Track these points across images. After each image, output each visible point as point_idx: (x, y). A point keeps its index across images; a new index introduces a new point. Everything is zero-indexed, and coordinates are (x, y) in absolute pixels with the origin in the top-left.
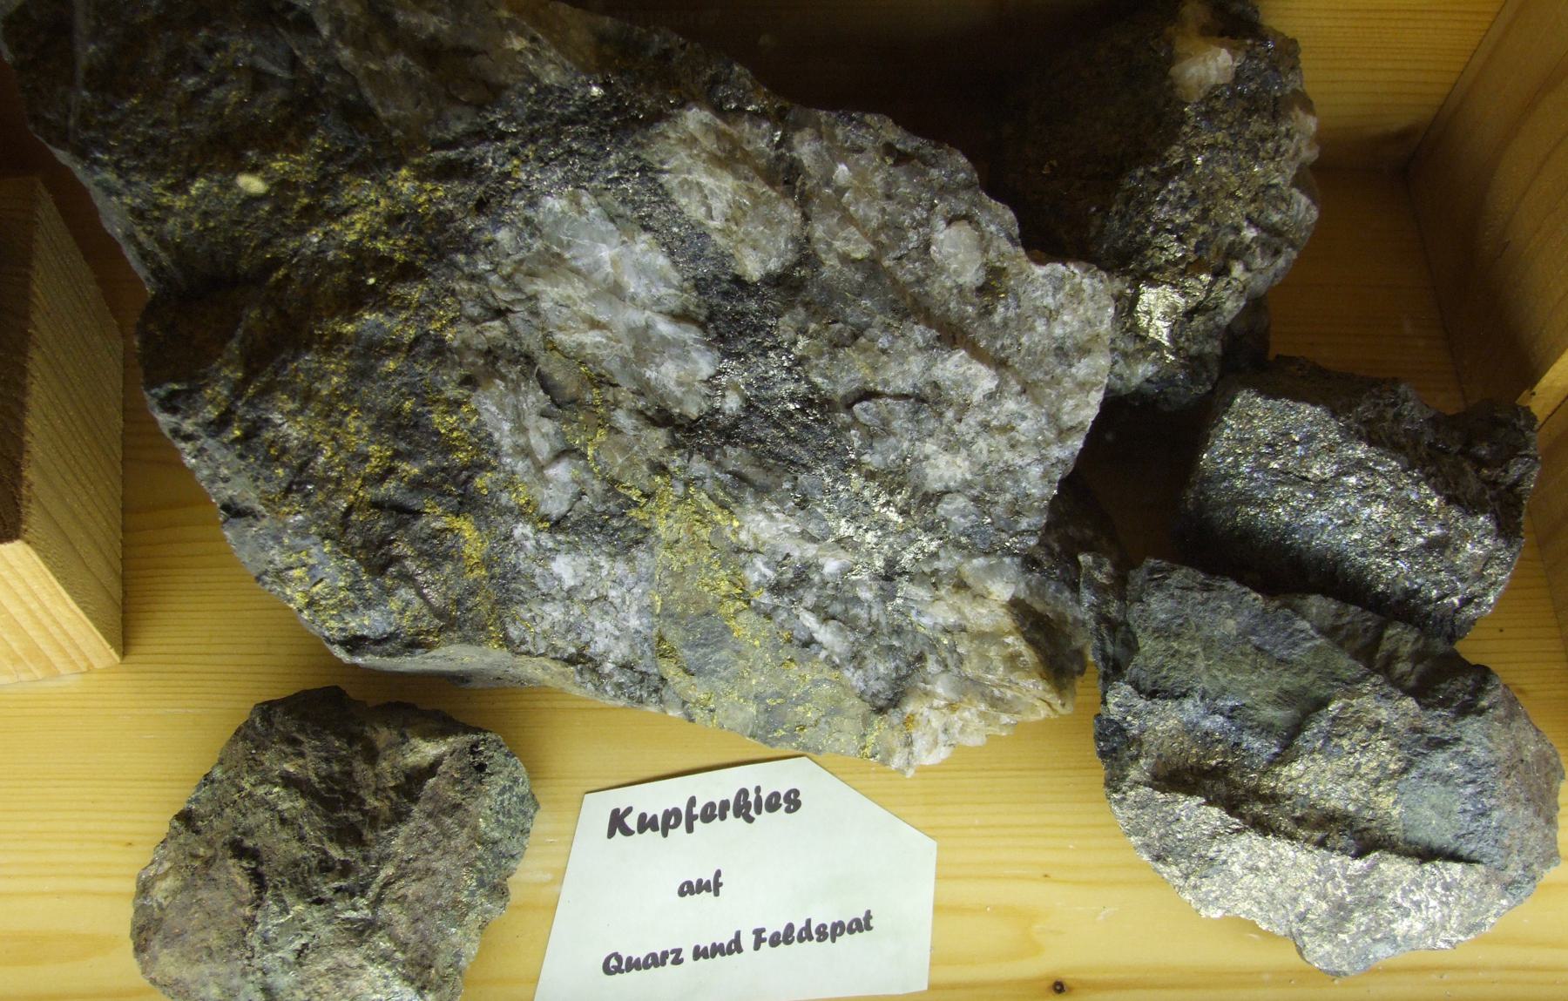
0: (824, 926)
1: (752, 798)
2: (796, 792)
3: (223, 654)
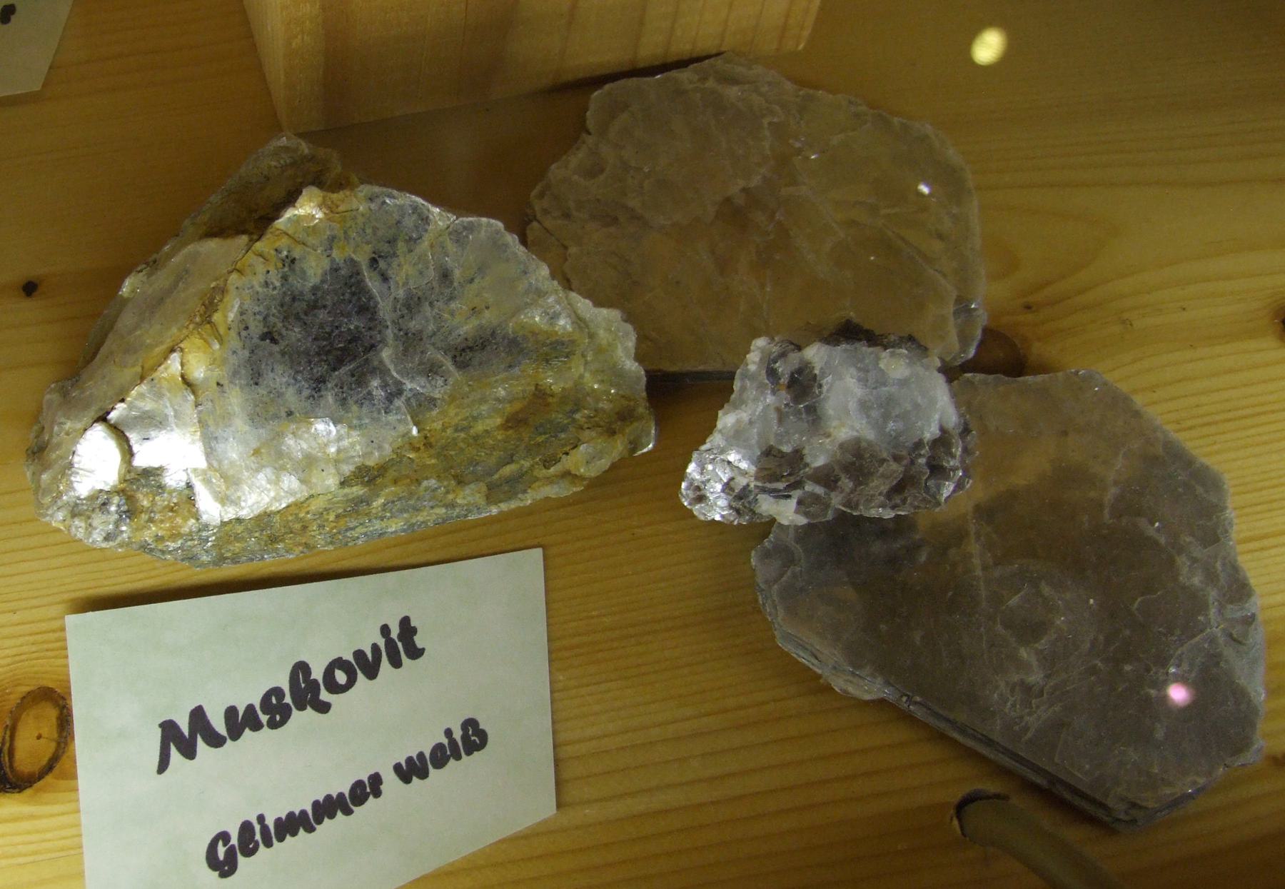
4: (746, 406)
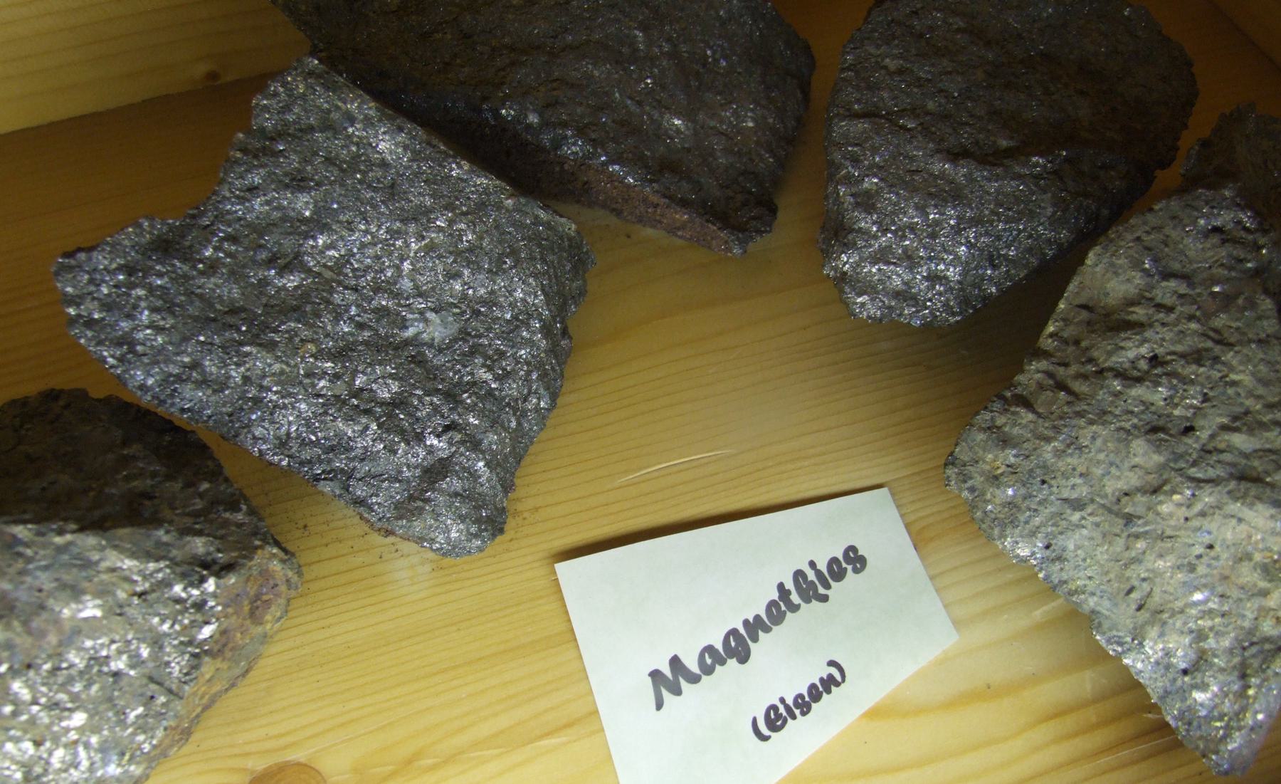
0: (801, 696)
1: (811, 576)
2: (852, 548)
3: (933, 514)
4: (1272, 517)
